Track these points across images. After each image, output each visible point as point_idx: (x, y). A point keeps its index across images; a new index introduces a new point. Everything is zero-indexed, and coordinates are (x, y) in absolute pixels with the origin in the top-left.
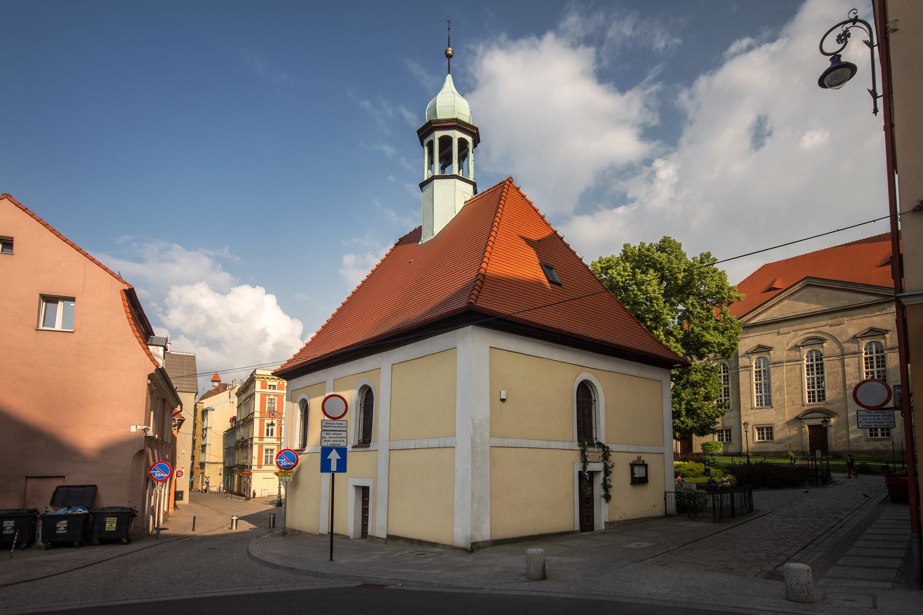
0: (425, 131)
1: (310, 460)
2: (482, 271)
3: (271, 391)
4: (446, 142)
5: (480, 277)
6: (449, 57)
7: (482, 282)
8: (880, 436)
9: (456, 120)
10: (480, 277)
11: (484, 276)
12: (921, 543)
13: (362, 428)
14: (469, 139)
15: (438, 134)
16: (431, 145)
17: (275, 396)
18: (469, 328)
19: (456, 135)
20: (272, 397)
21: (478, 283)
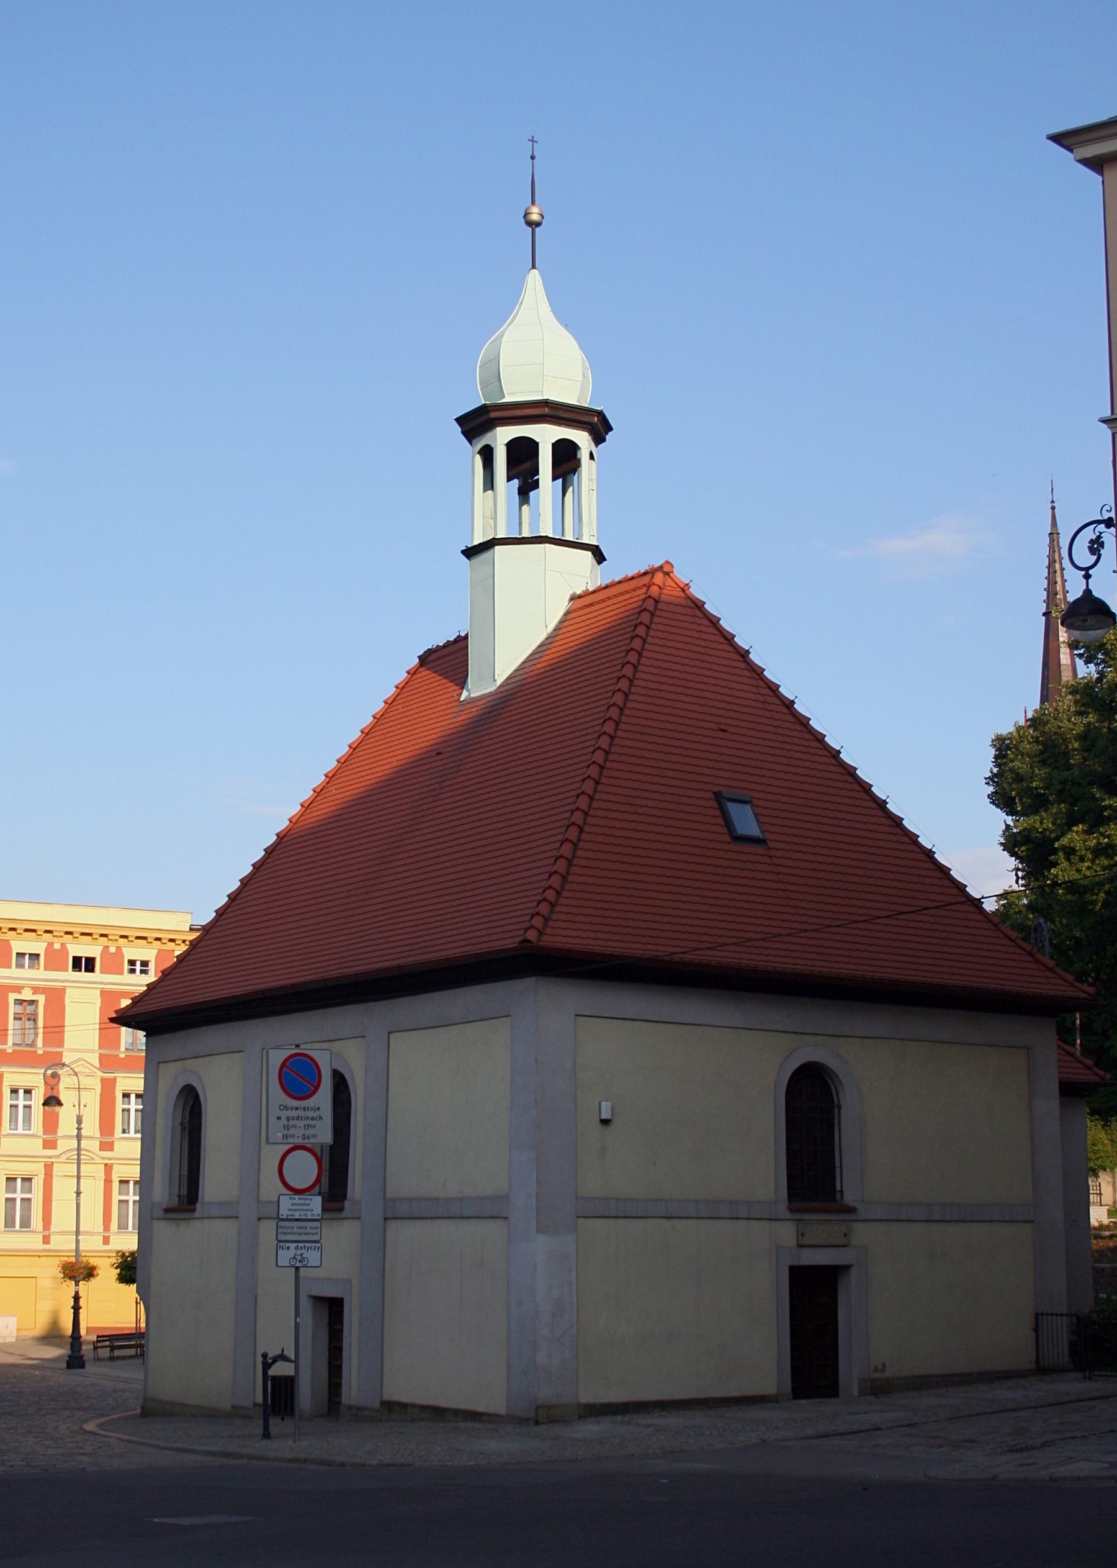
0: (476, 423)
1: (286, 1132)
2: (654, 591)
3: (27, 973)
4: (522, 454)
5: (650, 605)
6: (533, 225)
7: (546, 919)
8: (20, 1131)
9: (546, 403)
10: (650, 605)
11: (657, 602)
12: (1115, 1191)
13: (838, 1171)
14: (581, 438)
15: (502, 436)
16: (487, 454)
17: (36, 990)
18: (529, 983)
19: (546, 435)
20: (27, 995)
21: (645, 618)
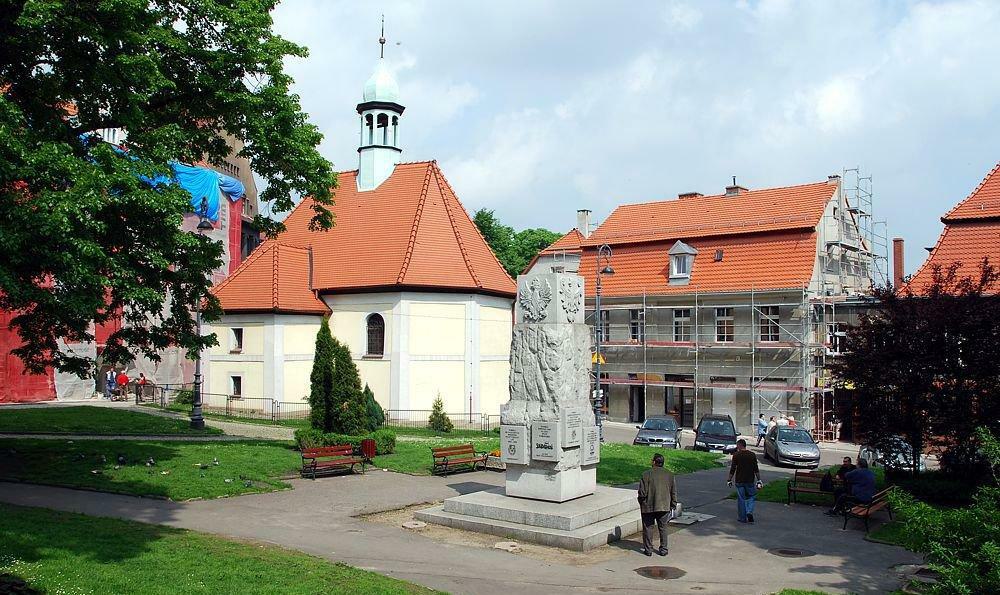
14: (397, 115)
16: (370, 118)
19: (390, 114)
